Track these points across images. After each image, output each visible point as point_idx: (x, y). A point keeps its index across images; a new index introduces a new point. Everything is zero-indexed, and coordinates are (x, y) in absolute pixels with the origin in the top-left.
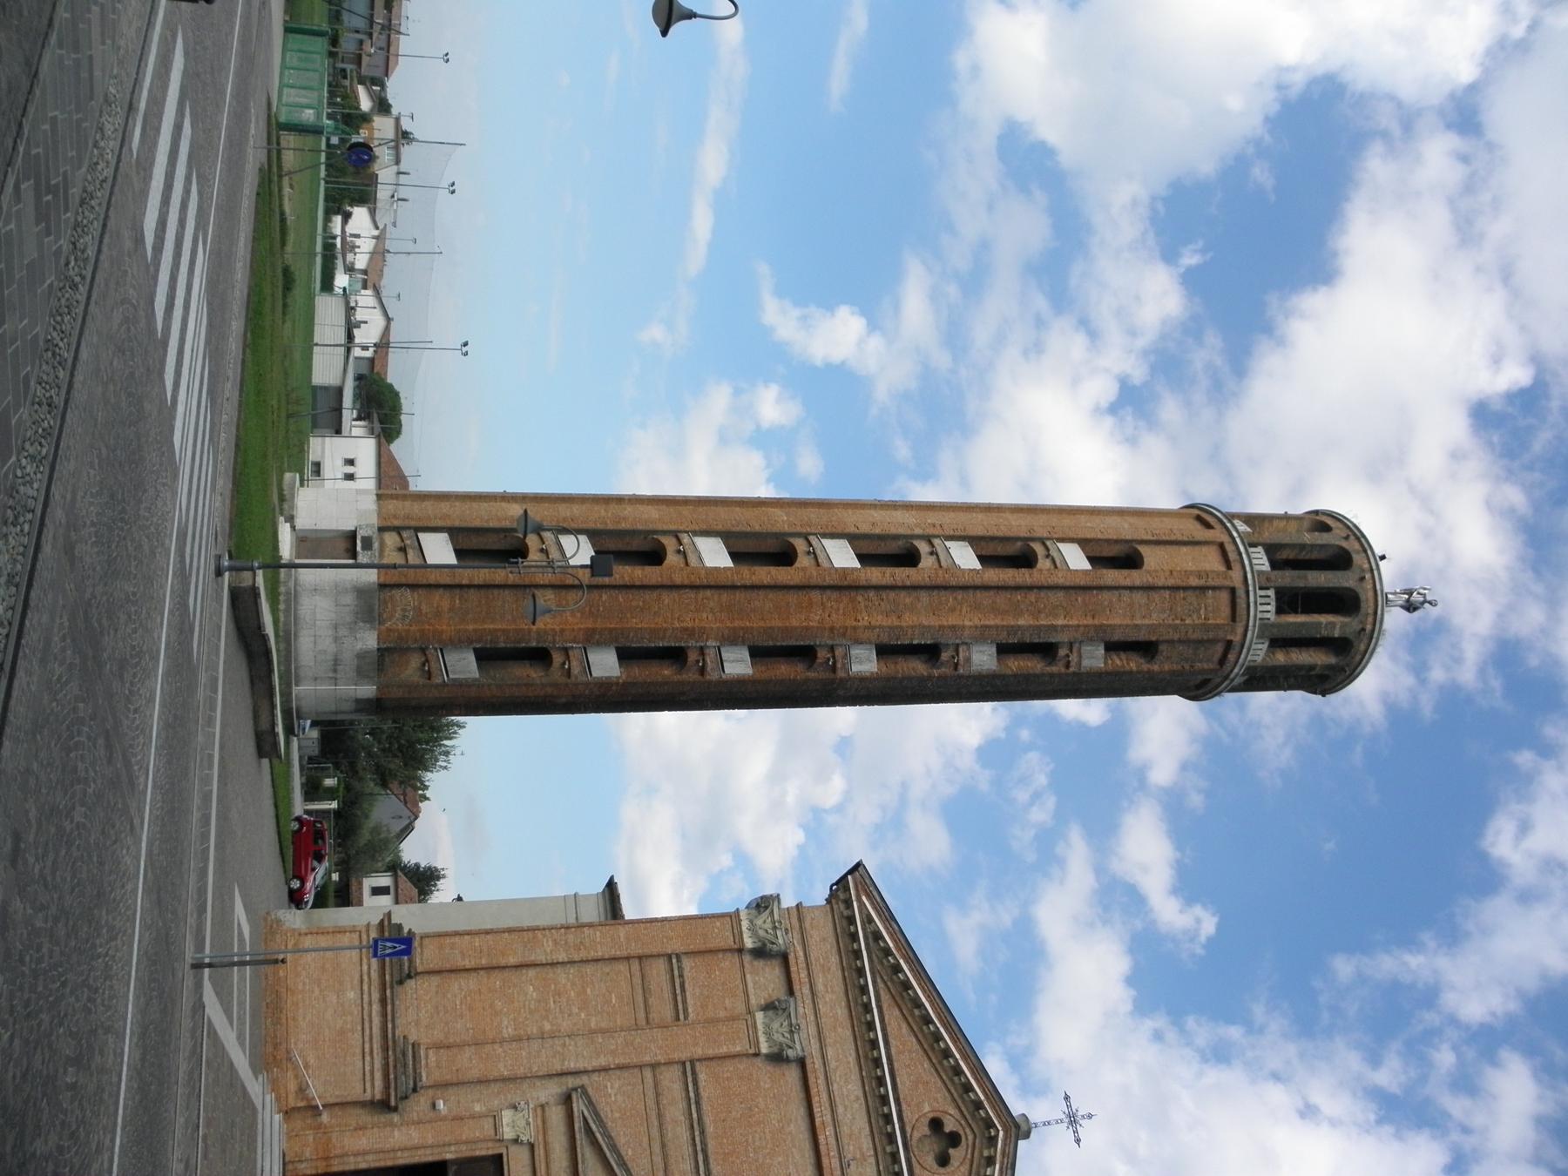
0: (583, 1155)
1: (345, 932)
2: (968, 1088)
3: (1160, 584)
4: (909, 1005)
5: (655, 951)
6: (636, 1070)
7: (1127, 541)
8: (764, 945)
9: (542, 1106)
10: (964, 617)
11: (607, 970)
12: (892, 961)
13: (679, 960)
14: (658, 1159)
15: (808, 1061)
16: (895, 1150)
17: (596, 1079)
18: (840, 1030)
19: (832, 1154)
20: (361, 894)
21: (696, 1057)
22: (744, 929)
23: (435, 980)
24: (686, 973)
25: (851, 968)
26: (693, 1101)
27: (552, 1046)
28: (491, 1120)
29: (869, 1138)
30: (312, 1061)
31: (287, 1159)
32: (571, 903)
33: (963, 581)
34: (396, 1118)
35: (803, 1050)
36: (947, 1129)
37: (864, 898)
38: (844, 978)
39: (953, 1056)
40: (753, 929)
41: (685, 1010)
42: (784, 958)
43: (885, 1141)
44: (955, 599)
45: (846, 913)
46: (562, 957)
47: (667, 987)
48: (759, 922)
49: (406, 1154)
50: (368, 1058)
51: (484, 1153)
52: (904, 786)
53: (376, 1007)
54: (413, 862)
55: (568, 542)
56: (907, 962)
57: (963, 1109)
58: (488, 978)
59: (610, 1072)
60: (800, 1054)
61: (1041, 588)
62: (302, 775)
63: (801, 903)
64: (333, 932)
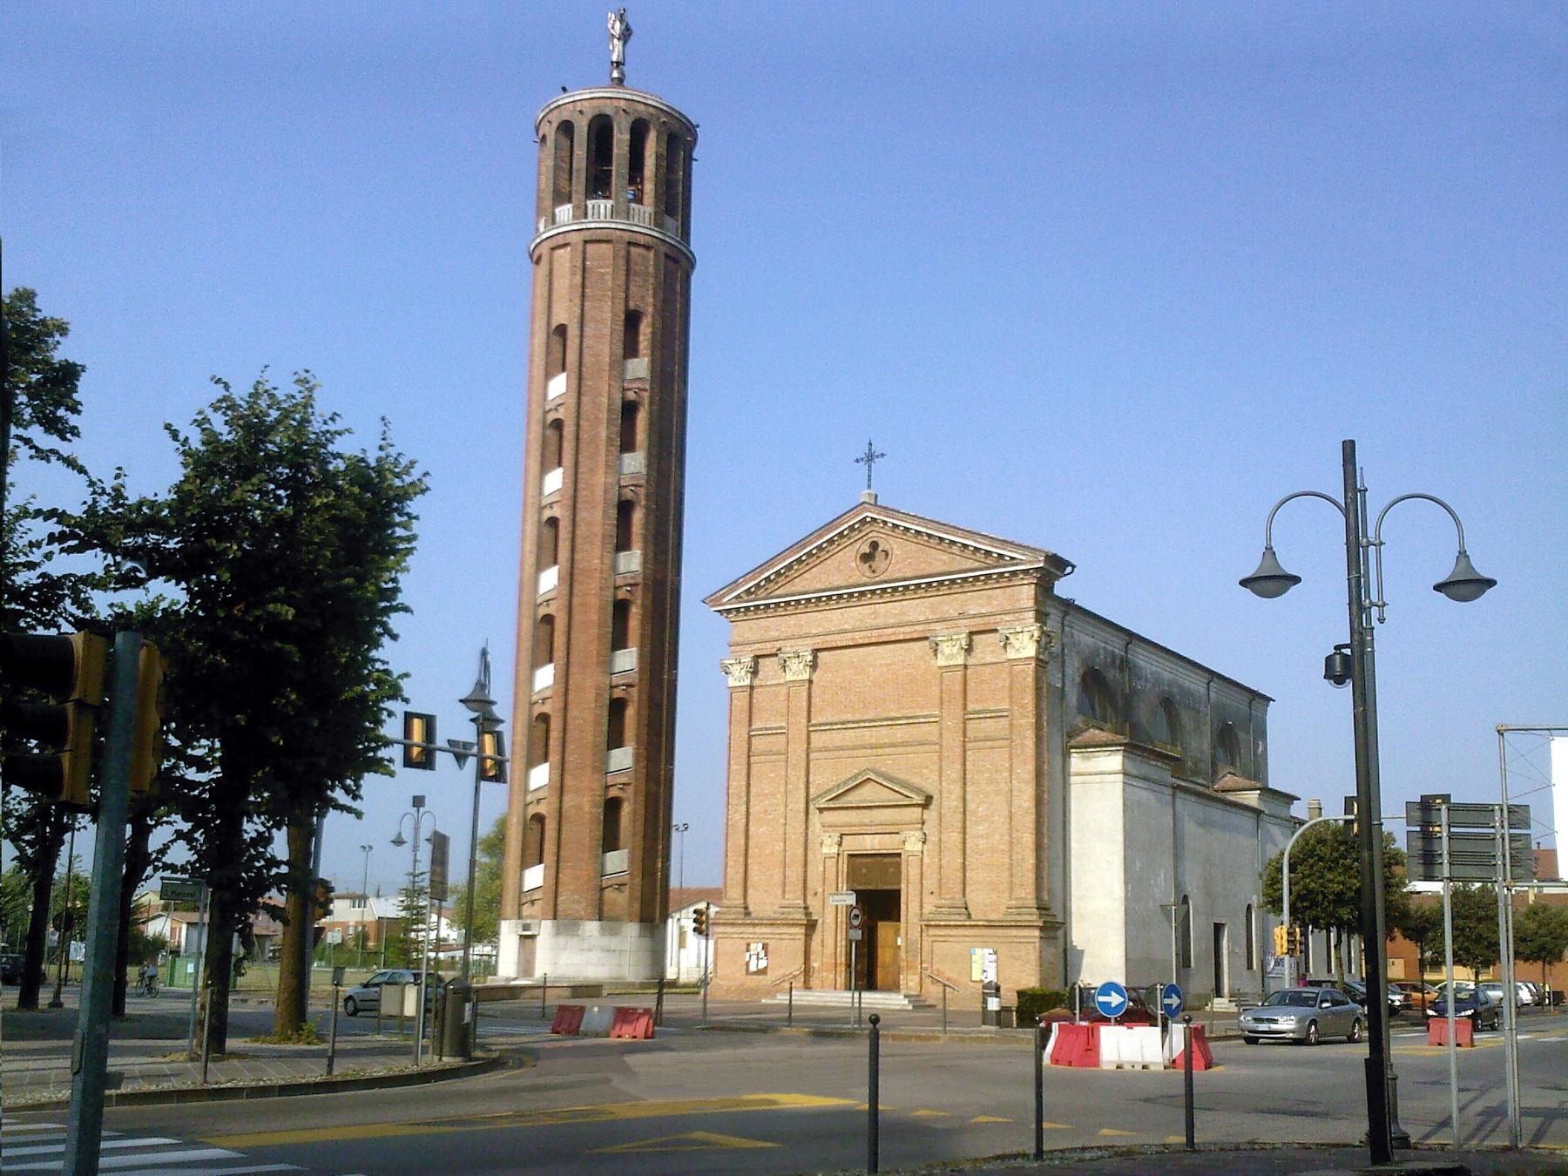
3: (579, 311)
7: (548, 337)
10: (599, 482)
13: (753, 731)
14: (862, 752)
33: (570, 485)
44: (584, 489)
50: (783, 936)
55: (533, 785)
61: (578, 417)
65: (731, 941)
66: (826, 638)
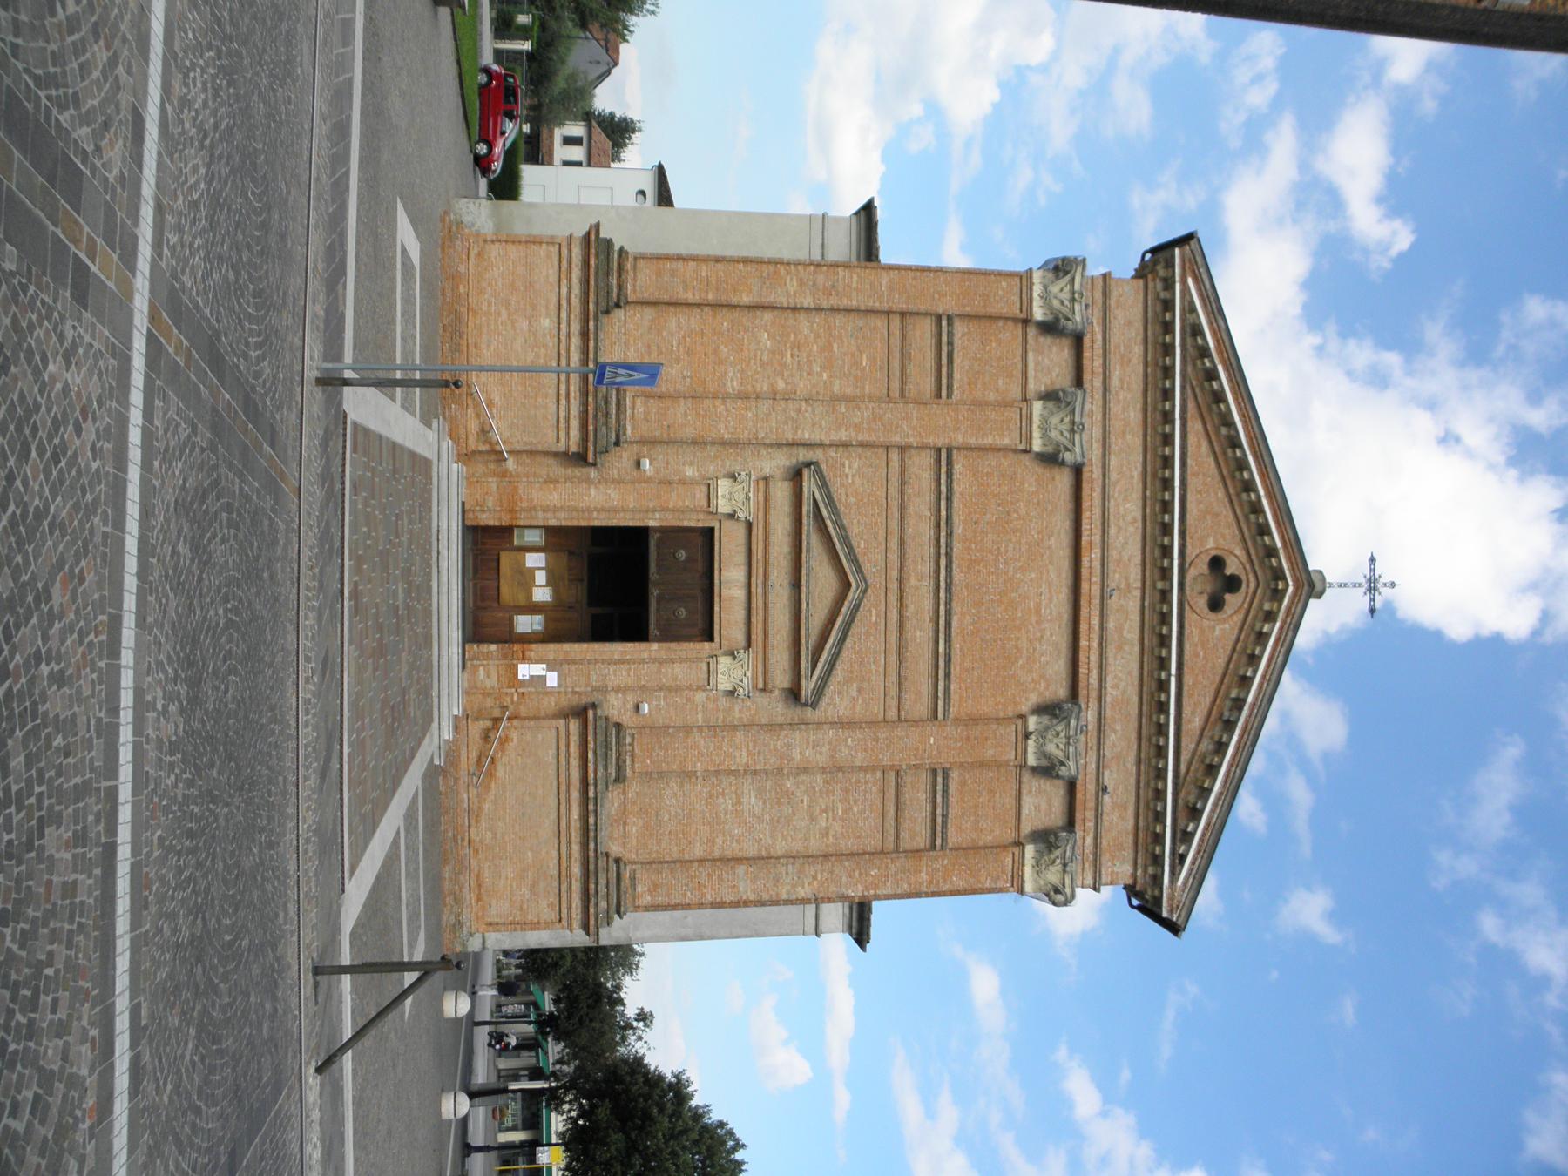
0: (808, 543)
1: (541, 243)
2: (1264, 530)
4: (1216, 421)
5: (923, 308)
6: (881, 450)
8: (1057, 320)
9: (766, 479)
11: (861, 323)
12: (1208, 364)
13: (950, 323)
14: (894, 557)
15: (1085, 470)
16: (1167, 588)
17: (833, 454)
18: (1129, 437)
19: (1094, 579)
20: (552, 143)
21: (955, 444)
22: (1035, 295)
23: (649, 313)
24: (957, 342)
25: (1157, 364)
26: (943, 496)
27: (784, 411)
28: (704, 489)
29: (1139, 568)
30: (497, 399)
31: (467, 507)
32: (818, 226)
34: (593, 473)
35: (1083, 457)
36: (1228, 572)
37: (1190, 281)
38: (1146, 375)
39: (1256, 491)
40: (1045, 297)
41: (950, 387)
42: (1078, 340)
43: (1157, 575)
45: (1163, 295)
46: (807, 301)
47: (930, 354)
48: (1055, 289)
49: (602, 516)
50: (563, 402)
51: (692, 524)
52: (1117, 51)
53: (576, 341)
54: (608, 111)
56: (1226, 369)
57: (1252, 551)
58: (714, 317)
59: (851, 449)
60: (1079, 459)
62: (491, 9)
63: (1110, 273)
64: (527, 242)
65: (553, 278)
66: (1098, 490)
